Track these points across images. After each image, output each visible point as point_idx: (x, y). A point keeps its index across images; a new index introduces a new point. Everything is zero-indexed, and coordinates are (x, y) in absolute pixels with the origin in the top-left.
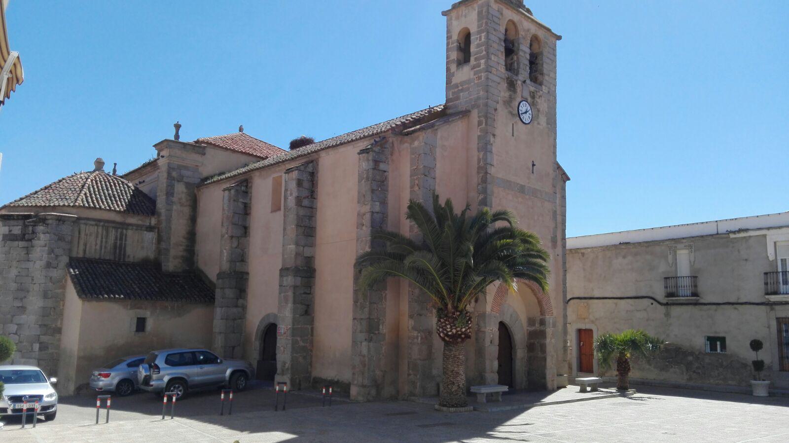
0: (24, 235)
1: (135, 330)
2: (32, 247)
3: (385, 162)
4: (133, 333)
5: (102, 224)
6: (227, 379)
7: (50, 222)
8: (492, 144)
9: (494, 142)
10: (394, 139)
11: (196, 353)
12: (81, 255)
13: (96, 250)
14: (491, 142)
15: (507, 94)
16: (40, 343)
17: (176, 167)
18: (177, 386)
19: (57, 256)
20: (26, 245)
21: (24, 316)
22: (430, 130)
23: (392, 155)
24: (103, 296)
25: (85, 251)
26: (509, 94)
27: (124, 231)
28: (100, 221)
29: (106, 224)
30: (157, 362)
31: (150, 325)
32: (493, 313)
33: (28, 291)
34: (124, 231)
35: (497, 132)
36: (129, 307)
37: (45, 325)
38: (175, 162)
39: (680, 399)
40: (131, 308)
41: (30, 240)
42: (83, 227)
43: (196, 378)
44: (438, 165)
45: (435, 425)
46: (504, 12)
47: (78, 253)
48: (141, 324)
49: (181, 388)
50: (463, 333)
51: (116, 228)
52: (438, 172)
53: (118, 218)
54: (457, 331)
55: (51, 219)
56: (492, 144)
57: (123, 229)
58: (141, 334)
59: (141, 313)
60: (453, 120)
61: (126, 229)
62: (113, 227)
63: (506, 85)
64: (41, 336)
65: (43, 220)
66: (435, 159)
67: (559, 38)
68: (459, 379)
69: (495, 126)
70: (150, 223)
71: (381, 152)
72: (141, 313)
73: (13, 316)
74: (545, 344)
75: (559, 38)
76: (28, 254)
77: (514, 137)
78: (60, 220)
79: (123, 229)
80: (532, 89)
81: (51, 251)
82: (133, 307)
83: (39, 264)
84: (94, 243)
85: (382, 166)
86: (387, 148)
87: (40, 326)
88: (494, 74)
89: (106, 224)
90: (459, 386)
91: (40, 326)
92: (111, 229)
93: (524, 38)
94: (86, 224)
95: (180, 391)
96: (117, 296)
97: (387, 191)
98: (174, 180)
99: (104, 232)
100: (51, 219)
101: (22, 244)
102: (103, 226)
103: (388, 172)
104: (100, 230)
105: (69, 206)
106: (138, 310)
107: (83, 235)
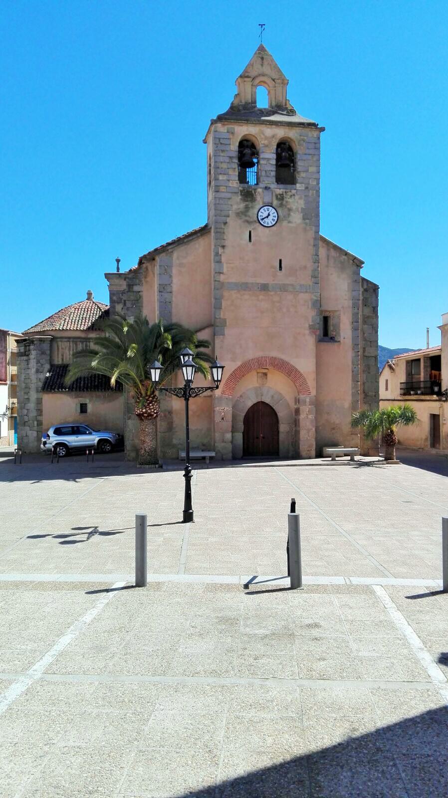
0: (25, 352)
1: (79, 411)
2: (29, 359)
3: (139, 285)
4: (78, 414)
5: (71, 340)
6: (96, 444)
7: (35, 342)
8: (221, 255)
9: (224, 252)
10: (148, 264)
11: (80, 428)
12: (60, 362)
13: (70, 358)
14: (220, 253)
15: (242, 206)
16: (37, 421)
17: (115, 293)
18: (64, 450)
19: (42, 365)
20: (27, 359)
21: (29, 404)
22: (164, 254)
23: (146, 278)
24: (62, 390)
25: (63, 359)
26: (244, 205)
27: (88, 343)
28: (69, 338)
29: (75, 340)
30: (49, 433)
31: (90, 408)
32: (224, 395)
33: (30, 388)
34: (88, 343)
35: (227, 243)
36: (74, 397)
37: (39, 410)
38: (114, 289)
39: (427, 473)
40: (76, 398)
41: (28, 355)
42: (60, 343)
43: (74, 444)
44: (175, 280)
45: (91, 473)
46: (236, 130)
47: (58, 361)
48: (83, 408)
49: (64, 450)
50: (144, 413)
51: (82, 342)
52: (175, 287)
53: (83, 335)
54: (151, 412)
55: (36, 340)
56: (221, 255)
57: (86, 342)
58: (84, 415)
59: (83, 400)
60: (192, 239)
61: (89, 342)
62: (81, 341)
63: (240, 197)
64: (37, 417)
65: (32, 342)
66: (171, 276)
67: (323, 129)
68: (145, 445)
69: (225, 238)
70: (105, 335)
71: (134, 277)
72: (83, 400)
73: (25, 404)
74: (299, 420)
75: (323, 129)
76: (28, 364)
77: (252, 243)
78: (41, 340)
79: (86, 342)
80: (279, 191)
81: (38, 362)
82: (77, 397)
83: (33, 370)
84: (68, 353)
85: (136, 288)
86: (142, 273)
87: (37, 410)
88: (223, 192)
89: (75, 340)
90: (145, 450)
91: (37, 410)
92: (78, 343)
93: (266, 146)
94: (62, 341)
95: (64, 451)
96: (64, 390)
97: (142, 307)
98: (115, 302)
99: (74, 345)
100: (36, 340)
101: (25, 358)
102: (73, 341)
103: (142, 292)
104: (71, 345)
105: (52, 330)
106: (80, 399)
107: (60, 348)
